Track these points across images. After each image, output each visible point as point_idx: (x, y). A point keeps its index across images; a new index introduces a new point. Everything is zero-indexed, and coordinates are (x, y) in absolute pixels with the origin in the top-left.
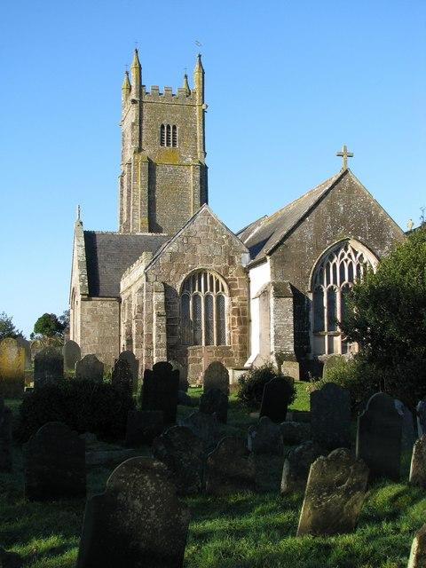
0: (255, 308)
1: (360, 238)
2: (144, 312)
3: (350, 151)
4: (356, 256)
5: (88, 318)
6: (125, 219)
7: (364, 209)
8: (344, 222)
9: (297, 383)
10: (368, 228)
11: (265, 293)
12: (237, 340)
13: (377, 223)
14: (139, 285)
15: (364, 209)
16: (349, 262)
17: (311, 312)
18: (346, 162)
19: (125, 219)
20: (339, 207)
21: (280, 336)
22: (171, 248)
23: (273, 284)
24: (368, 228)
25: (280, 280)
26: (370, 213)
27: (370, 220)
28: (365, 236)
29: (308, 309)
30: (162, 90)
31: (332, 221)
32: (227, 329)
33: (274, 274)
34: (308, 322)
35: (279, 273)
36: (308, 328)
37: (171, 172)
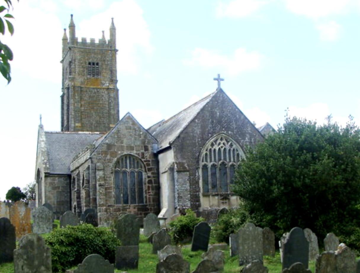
0: (165, 181)
1: (230, 132)
2: (91, 183)
3: (221, 77)
4: (227, 144)
5: (50, 189)
6: (65, 123)
7: (232, 114)
8: (220, 122)
9: (142, 242)
10: (234, 126)
11: (171, 169)
12: (151, 200)
13: (240, 123)
14: (86, 165)
15: (232, 114)
16: (223, 148)
17: (201, 181)
18: (219, 84)
19: (65, 123)
20: (216, 113)
21: (181, 197)
22: (107, 141)
23: (176, 163)
24: (234, 126)
25: (180, 160)
26: (235, 116)
27: (236, 121)
28: (233, 132)
29: (199, 179)
30: (88, 41)
31: (213, 122)
32: (144, 193)
33: (176, 157)
34: (198, 187)
35: (179, 156)
36: (199, 191)
37: (95, 93)
